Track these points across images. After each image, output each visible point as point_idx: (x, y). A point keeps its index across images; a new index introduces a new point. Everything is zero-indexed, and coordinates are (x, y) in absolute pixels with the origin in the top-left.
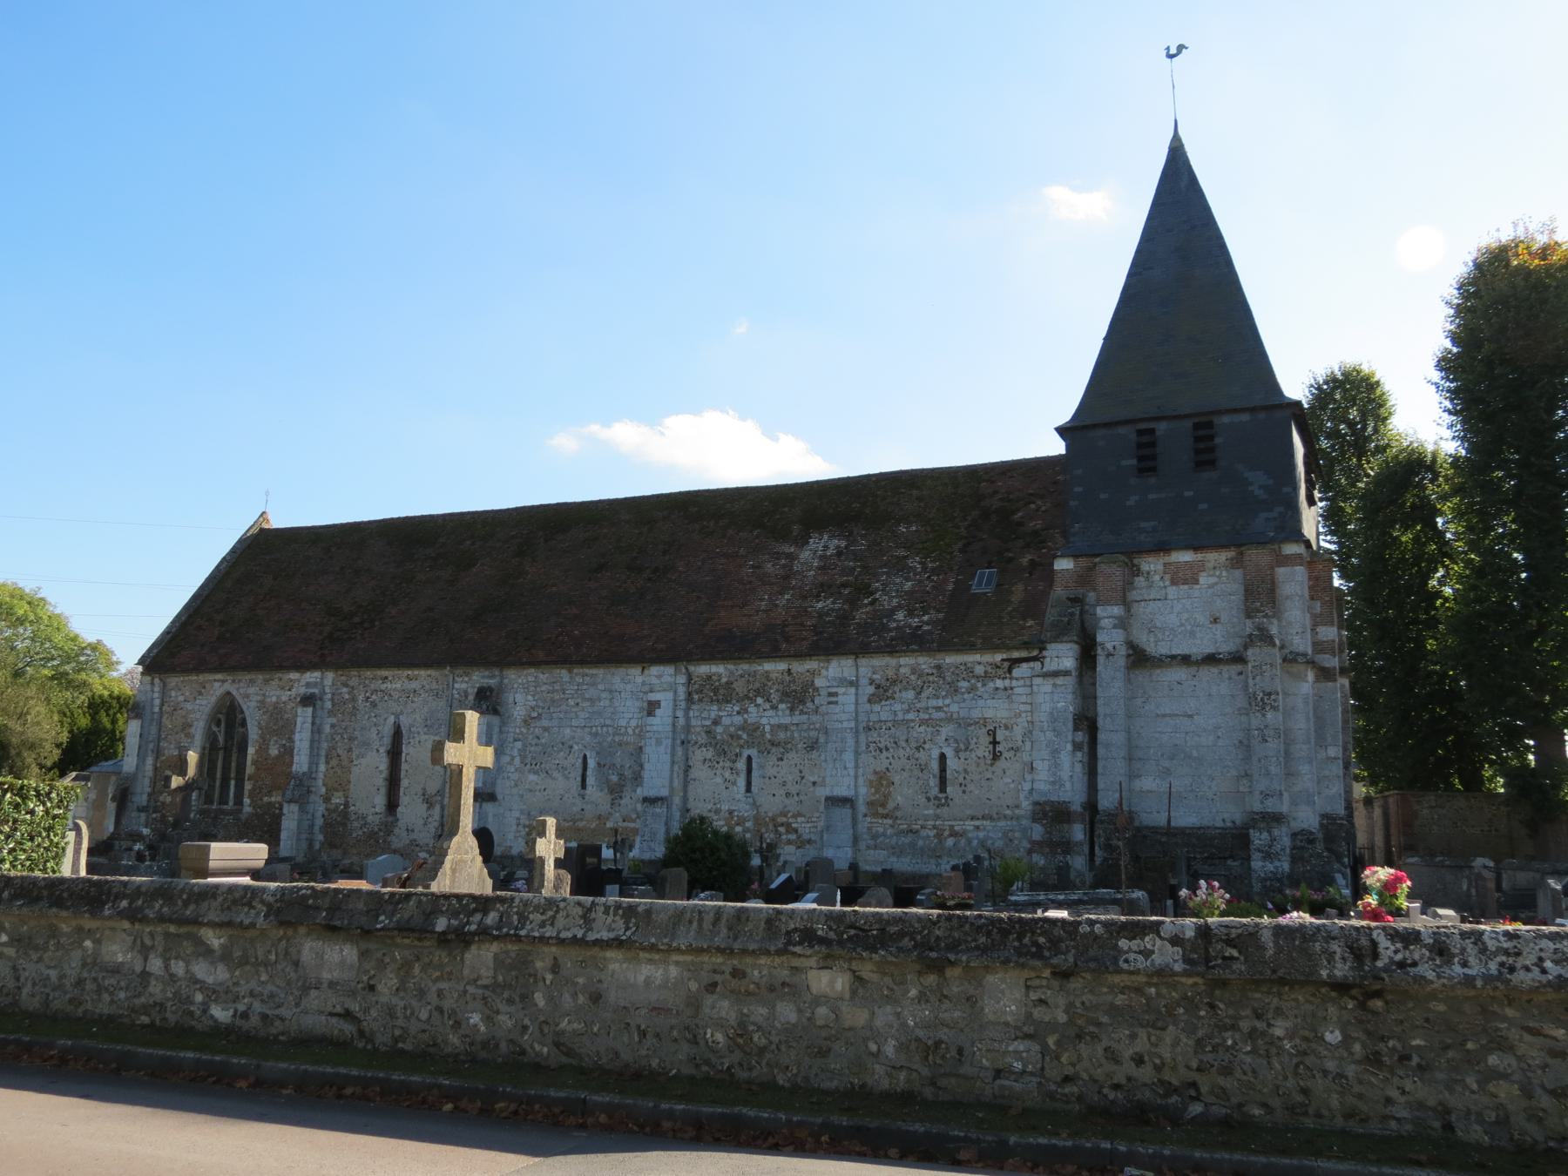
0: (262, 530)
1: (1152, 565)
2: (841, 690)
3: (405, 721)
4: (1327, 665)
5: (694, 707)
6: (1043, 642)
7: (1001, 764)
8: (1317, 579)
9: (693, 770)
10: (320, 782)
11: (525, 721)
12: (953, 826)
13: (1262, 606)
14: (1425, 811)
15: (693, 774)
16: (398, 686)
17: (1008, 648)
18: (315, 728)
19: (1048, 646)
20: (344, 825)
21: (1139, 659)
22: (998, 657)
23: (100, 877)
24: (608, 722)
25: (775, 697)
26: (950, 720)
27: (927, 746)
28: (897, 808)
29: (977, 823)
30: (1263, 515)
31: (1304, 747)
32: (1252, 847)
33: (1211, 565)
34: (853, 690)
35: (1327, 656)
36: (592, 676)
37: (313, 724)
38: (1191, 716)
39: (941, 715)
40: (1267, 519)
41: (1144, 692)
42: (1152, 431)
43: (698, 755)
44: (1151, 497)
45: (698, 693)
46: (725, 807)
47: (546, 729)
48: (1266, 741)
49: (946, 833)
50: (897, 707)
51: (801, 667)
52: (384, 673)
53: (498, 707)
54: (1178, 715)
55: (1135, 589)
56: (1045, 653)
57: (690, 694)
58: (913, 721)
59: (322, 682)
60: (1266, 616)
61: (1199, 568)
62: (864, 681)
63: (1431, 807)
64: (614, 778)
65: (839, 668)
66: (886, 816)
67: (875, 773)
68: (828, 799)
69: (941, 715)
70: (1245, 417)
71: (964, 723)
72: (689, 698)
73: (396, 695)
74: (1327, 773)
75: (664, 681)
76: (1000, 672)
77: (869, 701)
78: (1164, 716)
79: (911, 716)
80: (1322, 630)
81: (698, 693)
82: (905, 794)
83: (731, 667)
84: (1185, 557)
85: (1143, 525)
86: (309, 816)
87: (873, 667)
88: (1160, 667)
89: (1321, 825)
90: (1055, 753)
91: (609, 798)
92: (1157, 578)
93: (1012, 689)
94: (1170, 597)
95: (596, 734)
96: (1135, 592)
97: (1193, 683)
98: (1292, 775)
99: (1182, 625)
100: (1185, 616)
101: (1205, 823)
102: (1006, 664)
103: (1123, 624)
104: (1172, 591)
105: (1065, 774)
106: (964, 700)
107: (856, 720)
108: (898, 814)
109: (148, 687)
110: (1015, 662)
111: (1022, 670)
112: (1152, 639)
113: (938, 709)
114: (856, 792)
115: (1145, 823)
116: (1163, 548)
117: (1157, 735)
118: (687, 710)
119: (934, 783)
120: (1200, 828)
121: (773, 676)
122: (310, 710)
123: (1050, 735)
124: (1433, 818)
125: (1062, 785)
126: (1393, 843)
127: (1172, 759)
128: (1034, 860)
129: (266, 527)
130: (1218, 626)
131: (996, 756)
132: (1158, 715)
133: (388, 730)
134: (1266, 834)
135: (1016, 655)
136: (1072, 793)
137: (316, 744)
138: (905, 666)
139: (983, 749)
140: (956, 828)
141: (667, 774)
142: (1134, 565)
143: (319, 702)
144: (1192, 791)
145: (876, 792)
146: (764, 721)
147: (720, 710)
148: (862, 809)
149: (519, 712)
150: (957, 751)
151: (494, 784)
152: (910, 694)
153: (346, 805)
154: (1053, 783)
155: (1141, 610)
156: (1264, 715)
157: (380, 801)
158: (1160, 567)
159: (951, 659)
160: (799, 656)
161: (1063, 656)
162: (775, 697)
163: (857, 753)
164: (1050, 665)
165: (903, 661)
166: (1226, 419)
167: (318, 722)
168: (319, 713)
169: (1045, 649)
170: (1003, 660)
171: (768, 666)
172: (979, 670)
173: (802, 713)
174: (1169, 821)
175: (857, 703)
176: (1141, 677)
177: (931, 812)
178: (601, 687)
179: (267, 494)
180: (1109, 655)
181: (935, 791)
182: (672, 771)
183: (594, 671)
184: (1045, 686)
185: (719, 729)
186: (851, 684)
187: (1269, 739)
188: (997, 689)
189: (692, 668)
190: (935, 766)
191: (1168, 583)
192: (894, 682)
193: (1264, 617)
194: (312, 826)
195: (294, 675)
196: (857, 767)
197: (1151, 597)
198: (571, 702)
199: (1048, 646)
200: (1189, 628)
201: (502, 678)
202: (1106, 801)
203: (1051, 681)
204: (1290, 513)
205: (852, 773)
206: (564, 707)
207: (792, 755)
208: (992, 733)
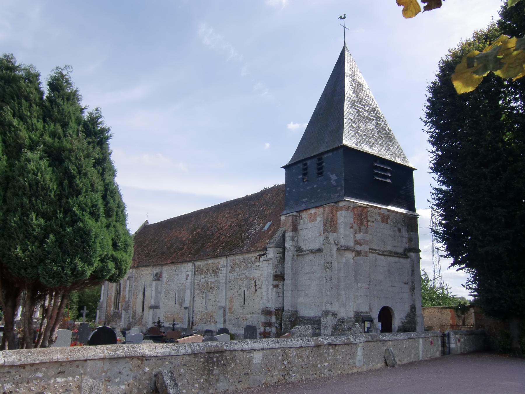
3: (146, 284)
5: (196, 276)
12: (246, 316)
15: (195, 299)
18: (131, 287)
21: (299, 250)
25: (211, 272)
26: (246, 278)
28: (234, 310)
32: (321, 324)
35: (358, 246)
38: (313, 273)
46: (201, 310)
56: (267, 252)
57: (195, 272)
60: (328, 232)
61: (316, 214)
64: (181, 300)
73: (145, 275)
75: (188, 268)
78: (307, 273)
80: (357, 235)
81: (198, 271)
92: (306, 220)
102: (259, 256)
104: (310, 224)
105: (270, 297)
107: (226, 279)
115: (301, 315)
117: (305, 281)
119: (242, 300)
120: (314, 317)
125: (269, 301)
126: (52, 308)
128: (267, 330)
131: (256, 291)
137: (131, 291)
139: (253, 289)
151: (159, 303)
154: (267, 300)
156: (327, 272)
158: (307, 216)
161: (272, 253)
163: (226, 290)
165: (237, 257)
166: (325, 156)
172: (253, 259)
174: (206, 309)
184: (266, 264)
185: (200, 284)
186: (225, 266)
190: (243, 294)
191: (309, 221)
194: (129, 317)
201: (162, 269)
203: (268, 262)
208: (255, 282)
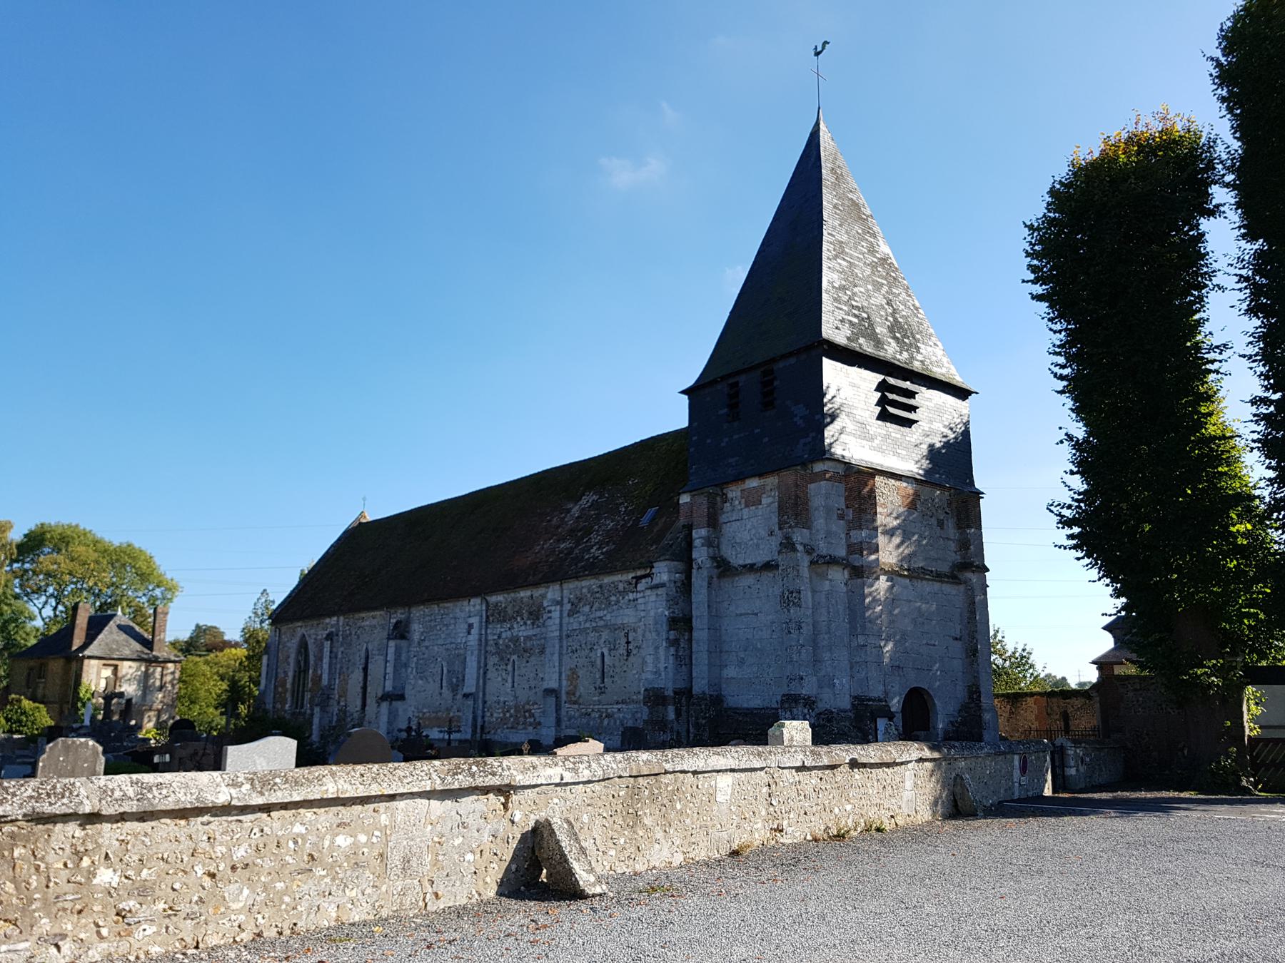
0: (360, 523)
1: (734, 492)
2: (553, 608)
4: (857, 564)
5: (490, 626)
6: (652, 563)
7: (631, 659)
8: (850, 489)
9: (489, 672)
10: (336, 692)
11: (419, 642)
13: (788, 518)
14: (1130, 694)
16: (368, 623)
17: (634, 569)
18: (333, 655)
19: (655, 565)
20: (344, 720)
21: (724, 568)
22: (631, 575)
23: (1070, 795)
24: (453, 641)
25: (525, 616)
27: (595, 647)
29: (619, 706)
30: (802, 441)
31: (826, 637)
33: (768, 488)
34: (558, 607)
36: (447, 608)
37: (331, 652)
38: (757, 614)
39: (602, 623)
40: (805, 444)
41: (729, 597)
42: (737, 383)
43: (493, 660)
44: (736, 437)
45: (494, 616)
47: (427, 647)
48: (791, 633)
49: (604, 715)
50: (582, 618)
51: (538, 592)
52: (363, 615)
53: (407, 634)
54: (748, 614)
55: (724, 513)
56: (654, 570)
58: (589, 628)
59: (338, 624)
61: (760, 491)
62: (566, 600)
63: (1136, 690)
65: (552, 592)
66: (575, 703)
67: (571, 669)
68: (546, 690)
69: (602, 623)
70: (792, 360)
71: (614, 628)
72: (487, 621)
74: (858, 659)
76: (632, 587)
77: (569, 615)
78: (741, 615)
79: (588, 625)
81: (494, 616)
82: (585, 687)
83: (506, 595)
84: (753, 483)
85: (731, 460)
86: (330, 715)
87: (571, 588)
88: (738, 575)
89: (853, 705)
90: (657, 648)
91: (451, 695)
92: (737, 502)
93: (637, 600)
94: (745, 517)
95: (447, 649)
96: (723, 516)
97: (759, 586)
98: (820, 662)
99: (752, 539)
100: (753, 531)
101: (766, 704)
102: (634, 580)
103: (709, 543)
106: (613, 611)
107: (561, 630)
108: (581, 701)
109: (273, 633)
110: (638, 579)
111: (642, 585)
112: (734, 553)
113: (601, 618)
114: (560, 685)
116: (741, 478)
118: (487, 628)
121: (525, 600)
122: (329, 642)
123: (654, 634)
124: (1138, 701)
127: (745, 651)
129: (364, 521)
130: (773, 538)
131: (629, 654)
132: (737, 615)
133: (363, 654)
134: (789, 713)
135: (639, 573)
136: (668, 683)
138: (585, 587)
140: (609, 711)
141: (475, 676)
142: (724, 494)
143: (335, 638)
144: (757, 677)
145: (571, 684)
146: (520, 634)
147: (501, 627)
148: (564, 697)
149: (416, 637)
150: (610, 650)
152: (587, 609)
153: (346, 706)
155: (728, 530)
156: (789, 611)
157: (359, 703)
159: (607, 580)
160: (536, 584)
162: (525, 616)
163: (561, 654)
164: (656, 581)
165: (584, 583)
166: (781, 364)
167: (334, 650)
168: (336, 644)
169: (653, 567)
170: (633, 578)
171: (522, 594)
172: (621, 587)
173: (538, 627)
175: (561, 618)
176: (726, 584)
177: (596, 698)
178: (451, 616)
179: (364, 499)
180: (700, 568)
181: (599, 681)
182: (479, 674)
183: (446, 605)
184: (651, 596)
185: (501, 642)
187: (792, 631)
188: (630, 600)
189: (488, 598)
190: (599, 662)
191: (743, 506)
192: (580, 600)
193: (789, 527)
195: (327, 620)
196: (560, 665)
197: (734, 519)
198: (438, 628)
199: (655, 565)
200: (755, 541)
202: (700, 686)
203: (655, 592)
204: (819, 436)
205: (557, 669)
206: (435, 632)
207: (533, 658)
208: (627, 635)
